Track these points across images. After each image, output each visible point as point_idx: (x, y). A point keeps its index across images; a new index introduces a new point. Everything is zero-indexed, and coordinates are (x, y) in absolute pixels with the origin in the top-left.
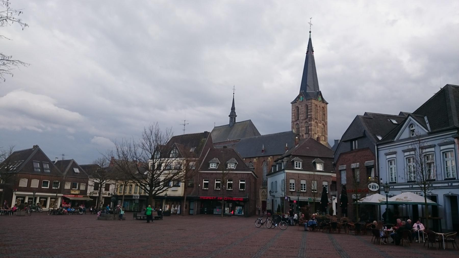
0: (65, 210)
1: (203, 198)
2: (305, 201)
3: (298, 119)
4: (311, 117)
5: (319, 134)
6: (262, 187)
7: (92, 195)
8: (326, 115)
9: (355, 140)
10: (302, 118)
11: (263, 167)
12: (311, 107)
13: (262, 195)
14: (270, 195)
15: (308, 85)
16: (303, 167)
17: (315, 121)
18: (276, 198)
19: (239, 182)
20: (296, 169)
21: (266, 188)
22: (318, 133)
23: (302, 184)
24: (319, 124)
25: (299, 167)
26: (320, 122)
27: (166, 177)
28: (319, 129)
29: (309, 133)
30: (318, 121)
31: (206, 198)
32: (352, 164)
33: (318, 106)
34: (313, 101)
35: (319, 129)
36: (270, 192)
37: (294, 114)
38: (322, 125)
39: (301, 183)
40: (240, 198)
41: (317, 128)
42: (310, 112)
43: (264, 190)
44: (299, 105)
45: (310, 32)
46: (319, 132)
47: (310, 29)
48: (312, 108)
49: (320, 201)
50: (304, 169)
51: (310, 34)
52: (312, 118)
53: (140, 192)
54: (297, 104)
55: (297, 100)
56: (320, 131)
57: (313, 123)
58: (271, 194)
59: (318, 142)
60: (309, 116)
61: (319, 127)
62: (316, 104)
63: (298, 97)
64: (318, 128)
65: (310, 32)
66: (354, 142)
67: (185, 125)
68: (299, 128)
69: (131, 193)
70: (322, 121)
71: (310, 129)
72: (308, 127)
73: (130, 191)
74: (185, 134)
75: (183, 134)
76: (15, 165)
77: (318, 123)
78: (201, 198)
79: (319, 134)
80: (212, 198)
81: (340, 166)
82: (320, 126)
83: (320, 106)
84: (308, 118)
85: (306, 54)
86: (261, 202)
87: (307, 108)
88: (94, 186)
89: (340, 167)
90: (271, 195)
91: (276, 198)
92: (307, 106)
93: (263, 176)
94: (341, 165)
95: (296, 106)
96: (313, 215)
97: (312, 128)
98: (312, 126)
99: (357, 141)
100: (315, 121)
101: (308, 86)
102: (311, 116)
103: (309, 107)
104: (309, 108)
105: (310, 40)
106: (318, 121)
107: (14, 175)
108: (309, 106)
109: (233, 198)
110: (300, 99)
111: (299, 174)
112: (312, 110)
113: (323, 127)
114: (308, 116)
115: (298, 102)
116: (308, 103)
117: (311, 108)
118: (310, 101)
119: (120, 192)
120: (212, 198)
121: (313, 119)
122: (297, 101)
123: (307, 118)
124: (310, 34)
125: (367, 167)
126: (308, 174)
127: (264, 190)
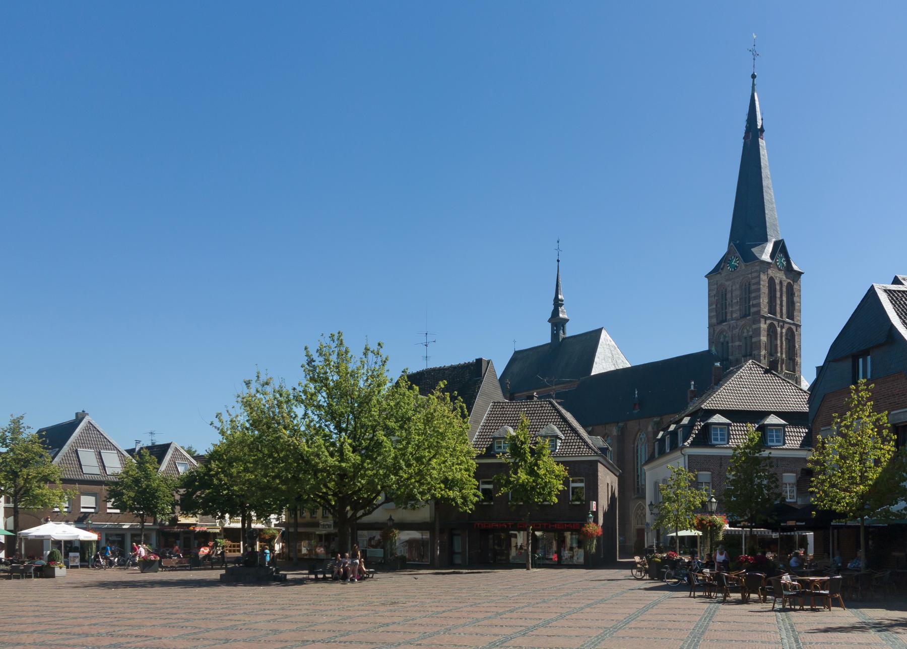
0: (678, 557)
1: (480, 526)
3: (724, 318)
6: (636, 496)
7: (229, 524)
8: (799, 304)
9: (864, 353)
10: (735, 316)
11: (637, 446)
13: (637, 514)
19: (569, 485)
21: (643, 497)
29: (753, 353)
36: (651, 504)
37: (714, 306)
40: (572, 524)
43: (640, 502)
44: (727, 280)
49: (554, 503)
51: (753, 81)
53: (325, 515)
55: (722, 266)
58: (653, 512)
60: (753, 310)
63: (725, 260)
65: (754, 76)
66: (861, 360)
67: (426, 345)
68: (727, 343)
69: (316, 517)
71: (755, 342)
72: (751, 337)
74: (429, 367)
75: (424, 368)
84: (749, 313)
85: (743, 140)
86: (862, 547)
89: (822, 430)
90: (654, 514)
93: (637, 469)
94: (825, 426)
99: (869, 358)
107: (283, 498)
109: (554, 524)
110: (728, 263)
113: (789, 338)
114: (749, 310)
115: (724, 273)
116: (751, 273)
119: (325, 515)
122: (722, 269)
123: (749, 315)
124: (753, 81)
127: (640, 502)
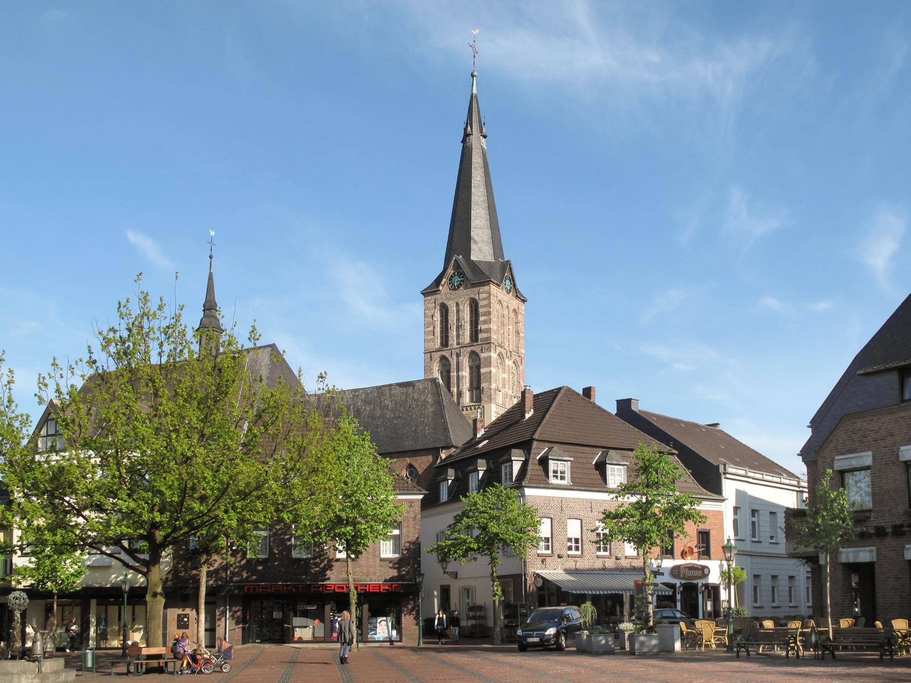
5: (506, 390)
12: (489, 305)
14: (445, 572)
18: (459, 579)
22: (504, 386)
23: (571, 539)
24: (507, 361)
26: (509, 354)
27: (298, 484)
28: (506, 376)
30: (504, 352)
31: (268, 588)
32: (902, 448)
35: (506, 376)
41: (500, 371)
42: (485, 322)
46: (507, 386)
52: (492, 341)
57: (494, 355)
58: (447, 571)
61: (507, 368)
62: (499, 298)
64: (504, 372)
65: (211, 257)
71: (485, 373)
76: (88, 629)
77: (505, 356)
79: (506, 390)
81: (837, 458)
88: (607, 465)
91: (459, 579)
92: (474, 306)
95: (438, 302)
96: (316, 606)
97: (490, 372)
100: (498, 349)
101: (476, 242)
102: (489, 335)
104: (481, 310)
105: (211, 275)
108: (481, 303)
111: (562, 500)
121: (493, 343)
125: (905, 462)
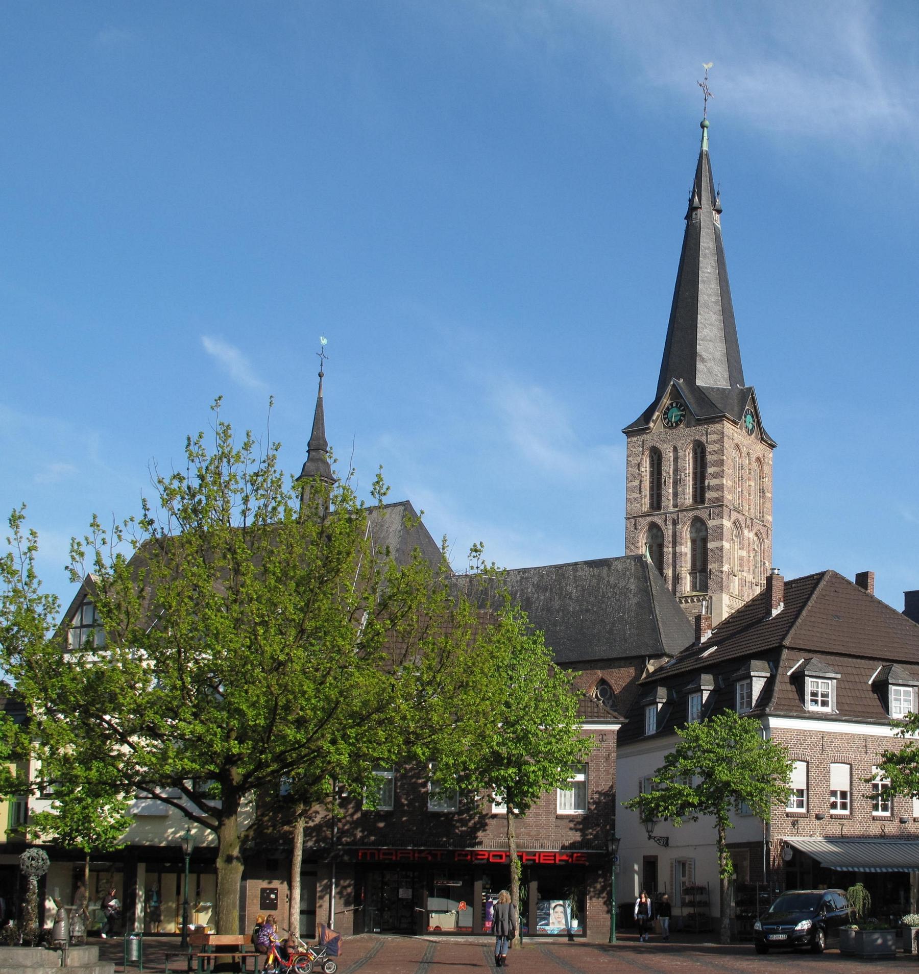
2: (873, 873)
4: (721, 499)
5: (745, 574)
14: (650, 837)
15: (700, 356)
16: (839, 704)
17: (733, 518)
20: (813, 712)
24: (746, 532)
25: (824, 704)
26: (749, 522)
28: (744, 553)
30: (741, 519)
33: (744, 450)
34: (728, 427)
35: (744, 553)
38: (756, 538)
39: (832, 788)
42: (715, 475)
45: (320, 375)
46: (746, 568)
47: (322, 365)
48: (725, 458)
50: (846, 713)
52: (725, 502)
54: (650, 439)
56: (748, 560)
57: (727, 523)
58: (653, 835)
59: (867, 595)
62: (736, 441)
70: (755, 520)
73: (401, 853)
76: (134, 905)
77: (744, 526)
78: (364, 854)
79: (745, 574)
80: (423, 855)
82: (749, 538)
83: (748, 454)
87: (699, 459)
95: (648, 445)
97: (722, 548)
98: (725, 538)
100: (734, 515)
101: (703, 360)
102: (720, 494)
103: (712, 453)
105: (320, 400)
106: (744, 518)
108: (710, 448)
111: (823, 735)
112: (727, 469)
117: (721, 458)
118: (718, 426)
120: (423, 855)
121: (727, 506)
126: (859, 737)
